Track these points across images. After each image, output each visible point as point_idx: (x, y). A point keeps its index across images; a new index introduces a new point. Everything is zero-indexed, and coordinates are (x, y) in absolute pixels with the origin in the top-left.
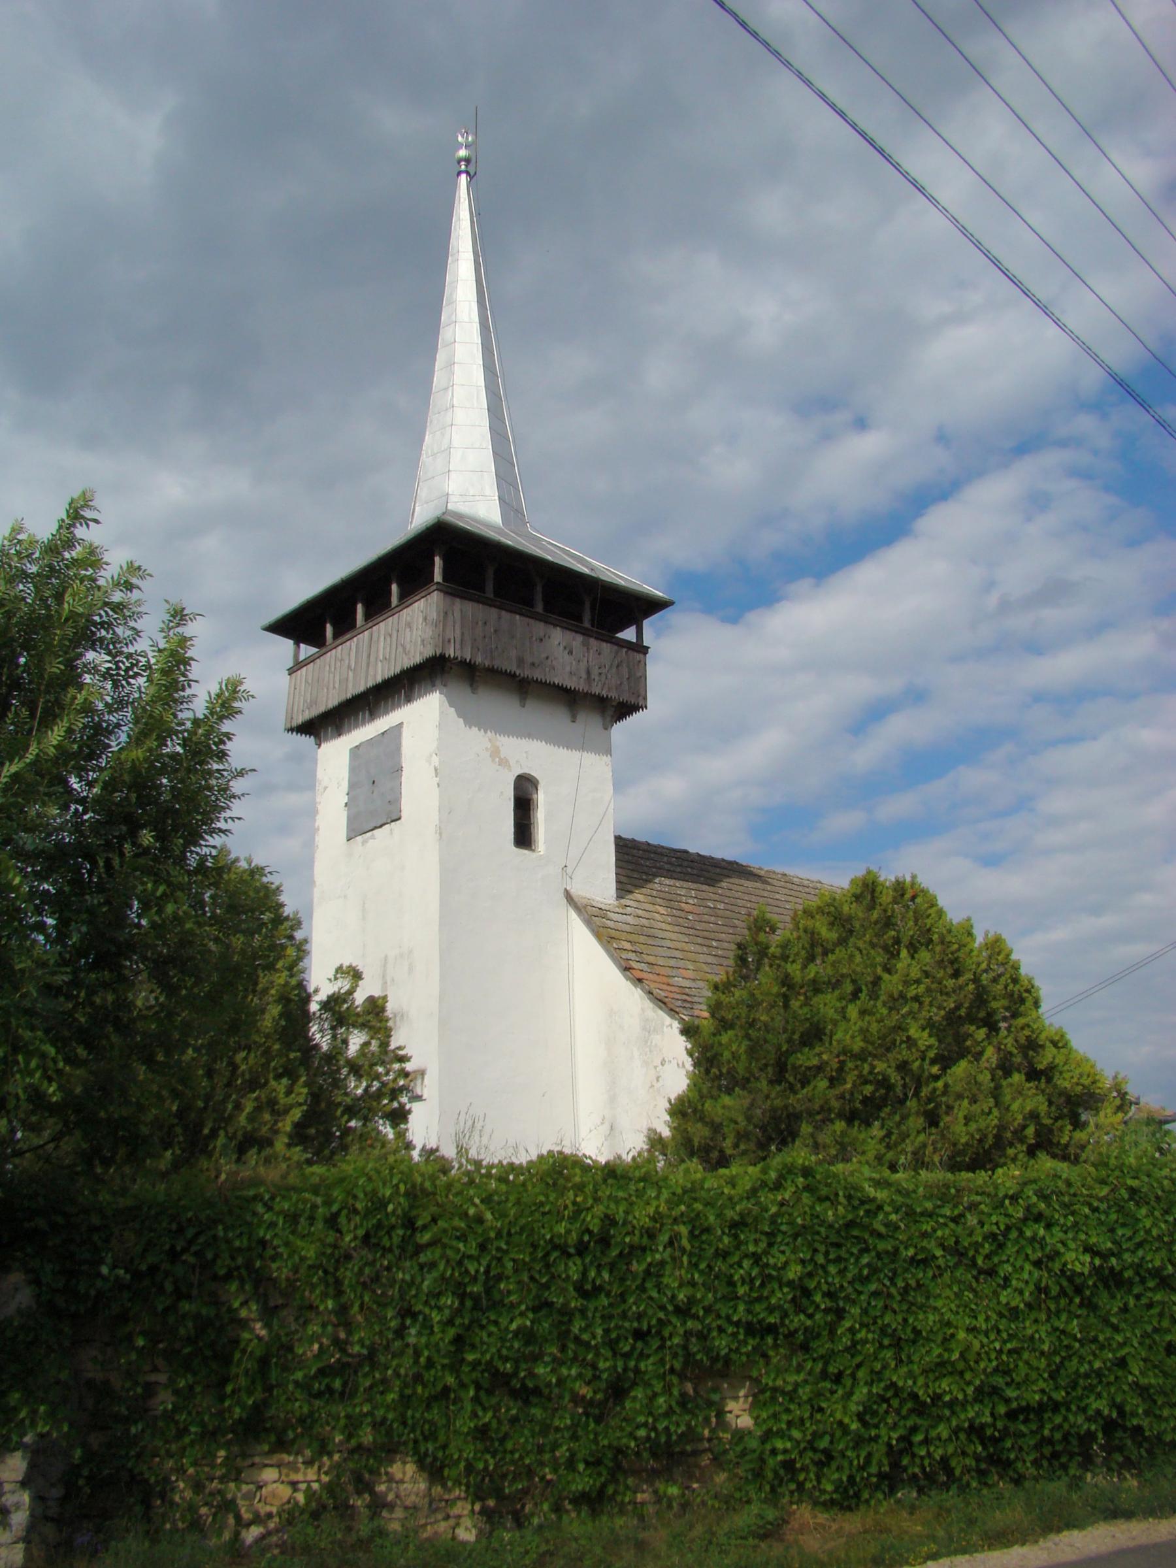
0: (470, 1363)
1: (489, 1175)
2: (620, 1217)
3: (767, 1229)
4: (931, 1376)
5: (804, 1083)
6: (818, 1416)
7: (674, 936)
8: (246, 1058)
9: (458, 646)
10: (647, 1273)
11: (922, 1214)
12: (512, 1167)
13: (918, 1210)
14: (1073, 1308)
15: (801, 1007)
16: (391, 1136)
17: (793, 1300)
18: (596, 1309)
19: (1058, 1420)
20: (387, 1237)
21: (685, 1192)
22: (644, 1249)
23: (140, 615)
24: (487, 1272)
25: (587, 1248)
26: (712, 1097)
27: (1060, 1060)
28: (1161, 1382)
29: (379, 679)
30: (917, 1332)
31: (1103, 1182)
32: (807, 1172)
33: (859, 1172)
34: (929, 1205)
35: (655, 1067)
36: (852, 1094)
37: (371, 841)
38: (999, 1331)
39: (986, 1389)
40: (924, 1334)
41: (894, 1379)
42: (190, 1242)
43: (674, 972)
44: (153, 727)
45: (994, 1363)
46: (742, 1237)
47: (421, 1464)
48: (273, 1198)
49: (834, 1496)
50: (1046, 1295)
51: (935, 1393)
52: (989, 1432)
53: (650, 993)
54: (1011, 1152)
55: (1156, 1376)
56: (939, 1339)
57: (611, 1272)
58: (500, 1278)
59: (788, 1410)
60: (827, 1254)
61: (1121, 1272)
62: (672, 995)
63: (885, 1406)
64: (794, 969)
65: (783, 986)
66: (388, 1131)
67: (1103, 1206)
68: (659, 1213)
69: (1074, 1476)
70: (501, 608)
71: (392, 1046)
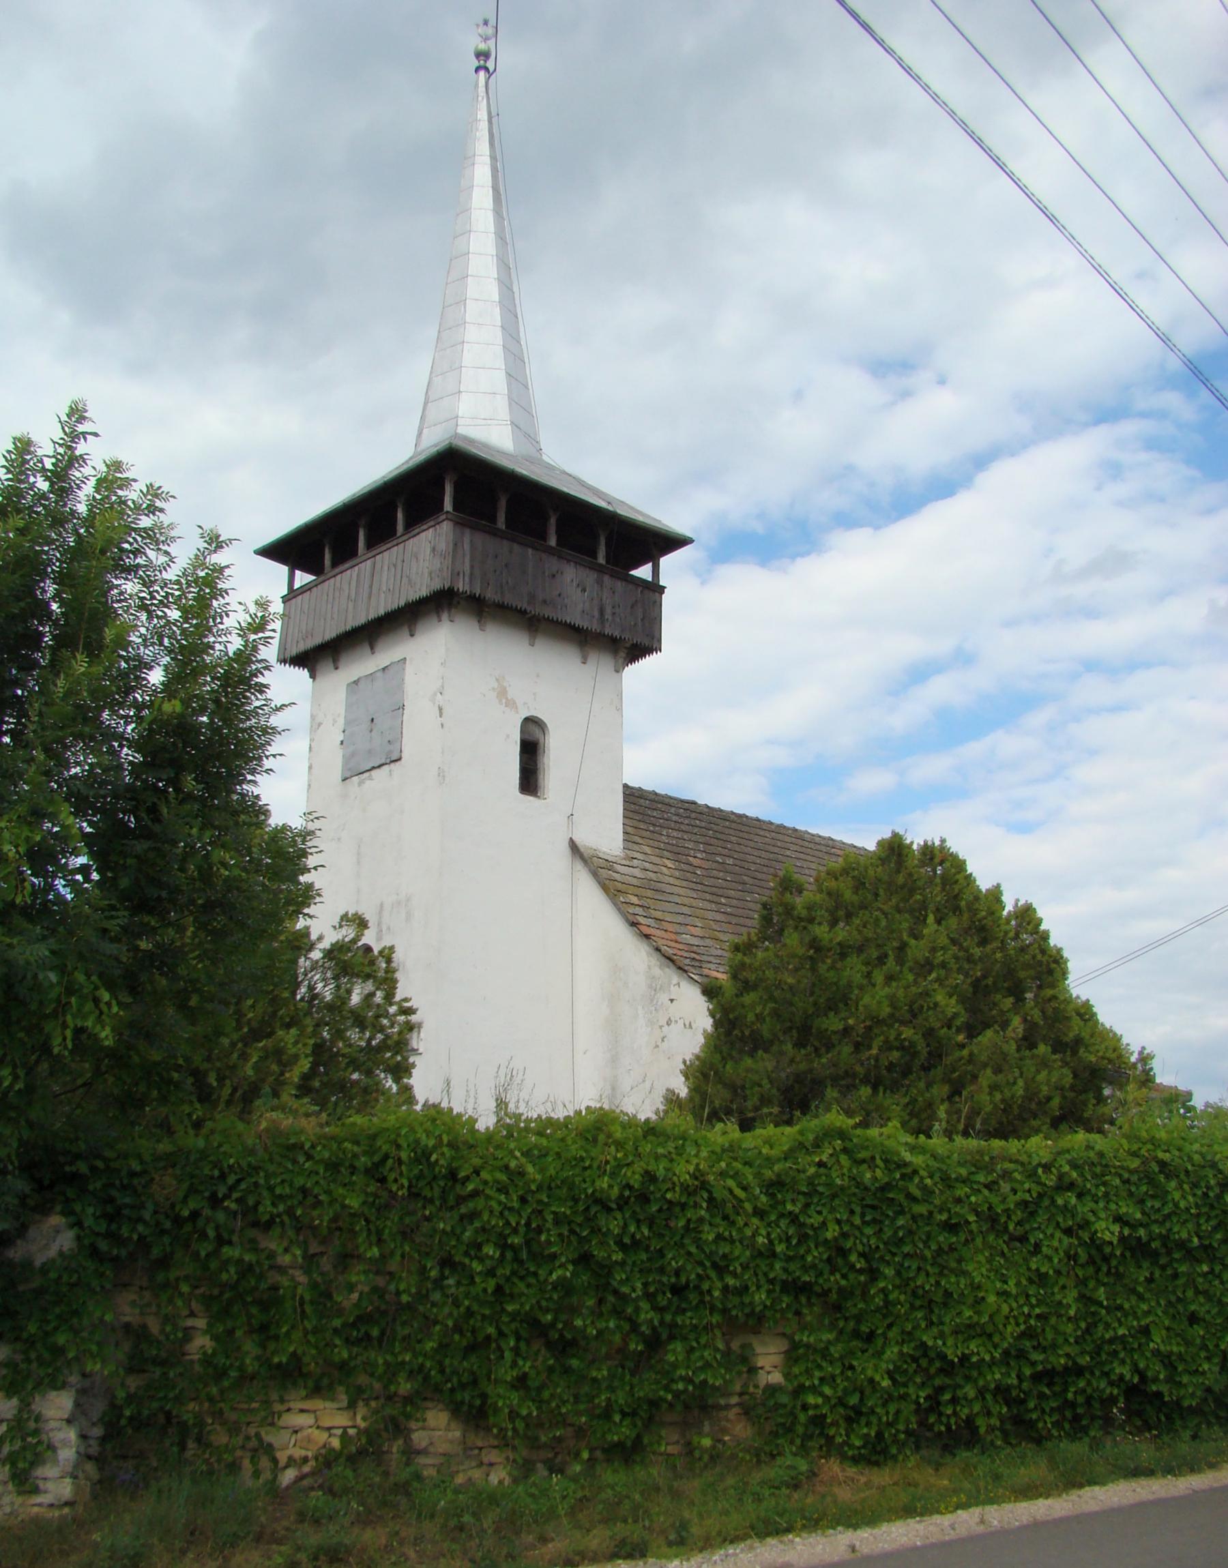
0: (509, 1314)
1: (527, 1129)
2: (661, 1173)
3: (804, 1189)
4: (960, 1337)
5: (829, 1047)
6: (849, 1373)
7: (682, 891)
8: (253, 1006)
9: (467, 579)
10: (687, 1228)
11: (957, 1179)
12: (550, 1122)
13: (953, 1176)
14: (1101, 1276)
15: (828, 970)
16: (395, 1088)
17: (829, 1260)
18: (634, 1262)
19: (1082, 1384)
20: (428, 1188)
21: (723, 1150)
22: (683, 1206)
23: (173, 539)
24: (528, 1224)
25: (626, 1203)
26: (732, 1058)
27: (1085, 1034)
28: (1182, 1350)
29: (382, 612)
30: (948, 1294)
31: (1135, 1154)
32: (842, 1134)
33: (891, 1135)
34: (963, 1172)
35: (661, 1027)
36: (877, 1060)
37: (368, 782)
38: (1028, 1296)
39: (1013, 1352)
40: (955, 1296)
41: (924, 1338)
42: (232, 1189)
43: (682, 929)
44: (189, 657)
45: (1023, 1327)
46: (779, 1196)
47: (456, 1410)
48: (313, 1147)
49: (863, 1451)
50: (1075, 1261)
51: (963, 1354)
52: (1014, 1393)
53: (658, 949)
54: (1035, 1123)
55: (1178, 1344)
56: (970, 1300)
57: (650, 1228)
58: (539, 1230)
59: (819, 1367)
60: (863, 1215)
61: (1149, 1242)
62: (680, 953)
63: (914, 1365)
64: (821, 931)
65: (811, 947)
66: (390, 1084)
67: (1134, 1178)
68: (699, 1170)
69: (1094, 1437)
70: (513, 540)
71: (398, 998)
